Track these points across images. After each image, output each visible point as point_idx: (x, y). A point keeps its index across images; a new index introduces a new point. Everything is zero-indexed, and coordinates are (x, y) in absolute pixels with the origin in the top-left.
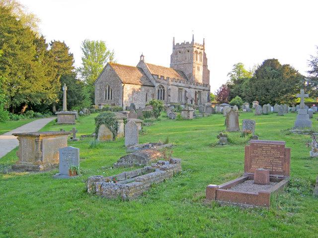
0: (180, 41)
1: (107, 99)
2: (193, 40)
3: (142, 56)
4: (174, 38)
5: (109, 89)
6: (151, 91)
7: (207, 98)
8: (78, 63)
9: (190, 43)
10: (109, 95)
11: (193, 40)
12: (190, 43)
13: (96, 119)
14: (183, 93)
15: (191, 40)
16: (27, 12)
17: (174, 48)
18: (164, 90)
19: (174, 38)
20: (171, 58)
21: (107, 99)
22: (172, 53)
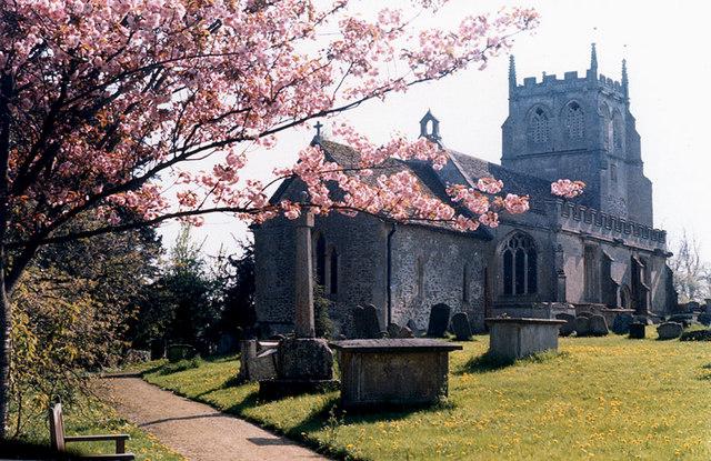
9: (582, 75)
12: (582, 75)
18: (533, 254)
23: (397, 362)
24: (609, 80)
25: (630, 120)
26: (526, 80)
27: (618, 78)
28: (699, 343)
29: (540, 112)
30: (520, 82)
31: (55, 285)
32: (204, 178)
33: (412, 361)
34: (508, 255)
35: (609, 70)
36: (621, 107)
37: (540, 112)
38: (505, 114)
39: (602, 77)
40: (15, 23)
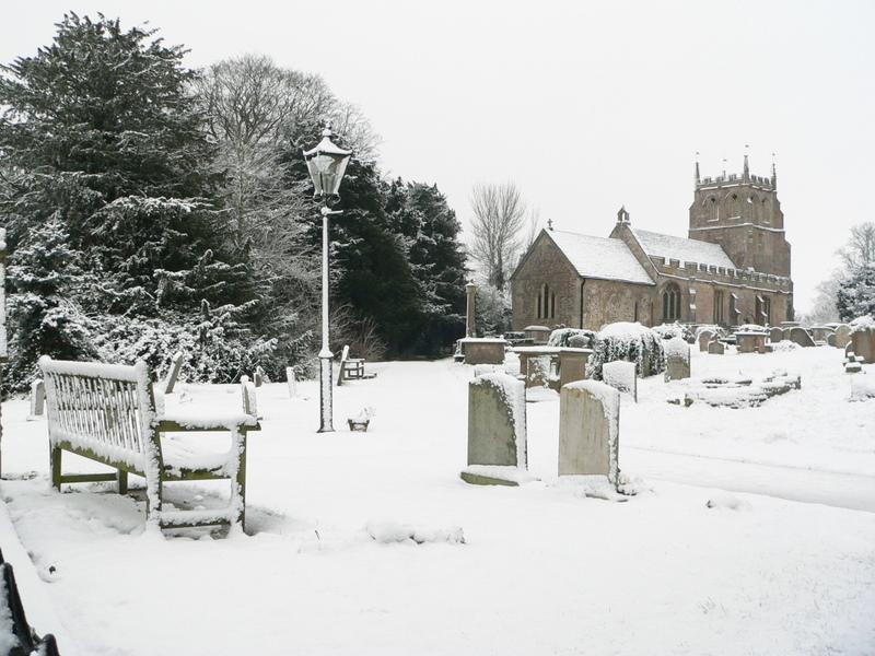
0: (712, 172)
1: (542, 316)
2: (747, 170)
3: (622, 212)
4: (514, 484)
5: (546, 293)
6: (646, 296)
7: (785, 312)
8: (24, 82)
9: (739, 176)
10: (546, 307)
11: (747, 170)
12: (739, 176)
13: (678, 262)
14: (727, 302)
15: (742, 171)
16: (260, 56)
17: (698, 191)
18: (679, 295)
19: (514, 484)
20: (691, 214)
21: (542, 316)
22: (693, 201)
23: (483, 348)
24: (760, 179)
25: (777, 204)
26: (706, 180)
27: (770, 177)
28: (615, 278)
29: (713, 200)
30: (702, 179)
31: (107, 335)
32: (500, 288)
33: (489, 347)
34: (666, 295)
35: (760, 171)
36: (770, 197)
37: (713, 200)
38: (692, 200)
39: (754, 178)
40: (869, 361)
